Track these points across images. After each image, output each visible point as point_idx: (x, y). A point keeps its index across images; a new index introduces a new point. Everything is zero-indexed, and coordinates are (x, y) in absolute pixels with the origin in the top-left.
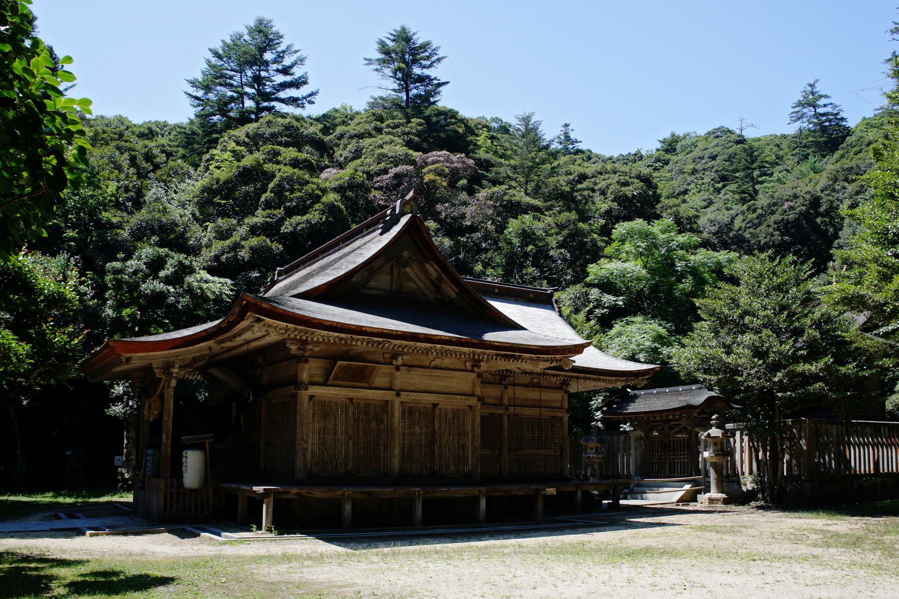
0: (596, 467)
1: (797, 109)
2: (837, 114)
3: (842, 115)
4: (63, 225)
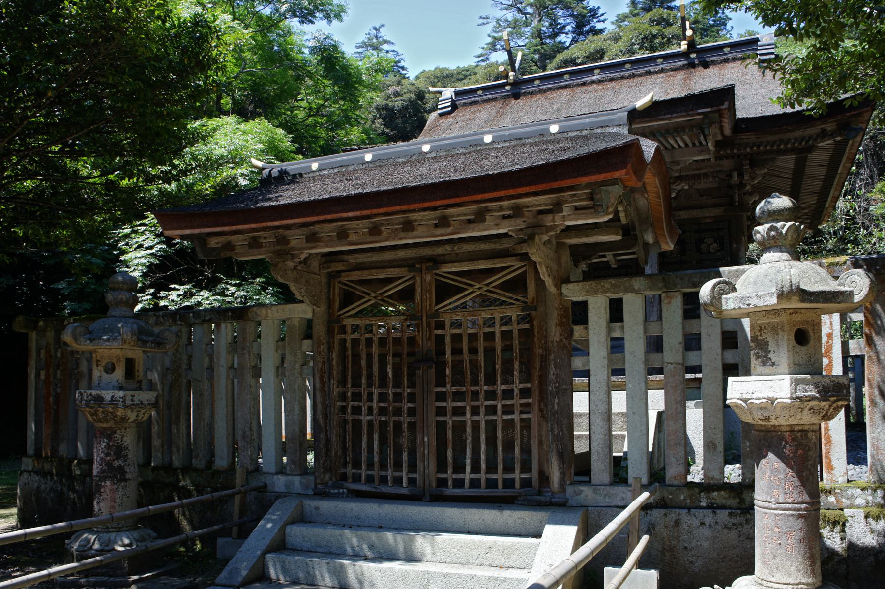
0: (128, 439)
1: (360, 50)
2: (399, 62)
3: (402, 64)
4: (251, 108)
